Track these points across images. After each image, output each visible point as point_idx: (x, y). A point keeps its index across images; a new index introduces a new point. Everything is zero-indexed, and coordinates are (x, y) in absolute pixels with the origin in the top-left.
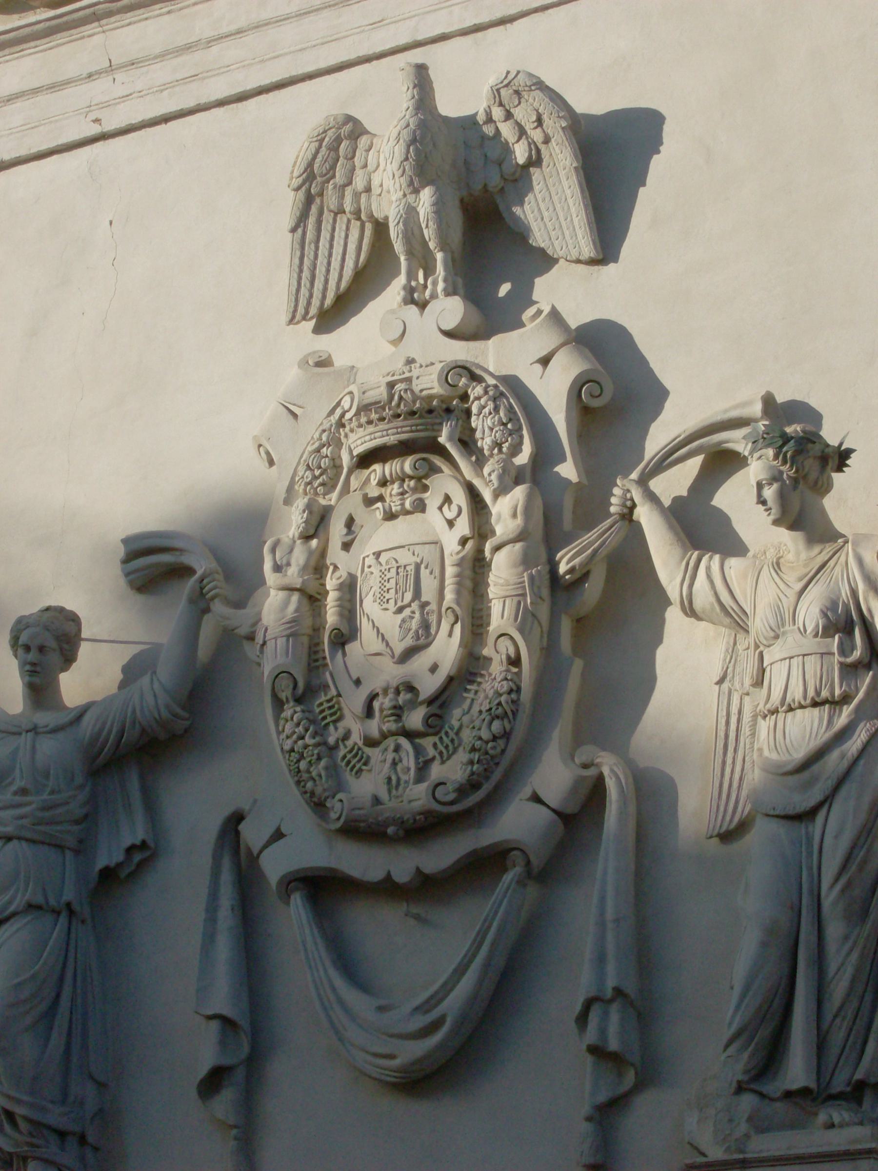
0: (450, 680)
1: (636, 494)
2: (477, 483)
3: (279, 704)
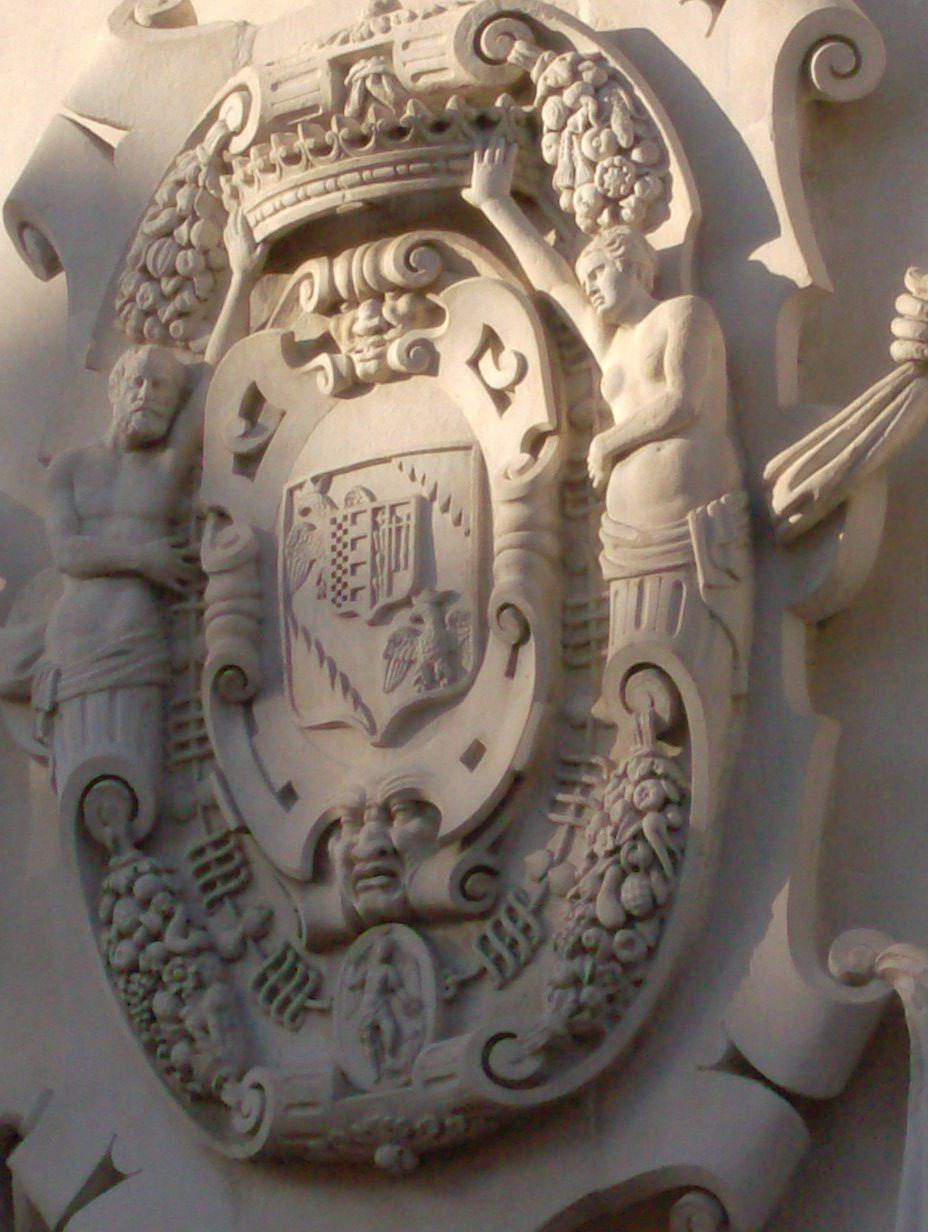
0: (516, 780)
2: (561, 295)
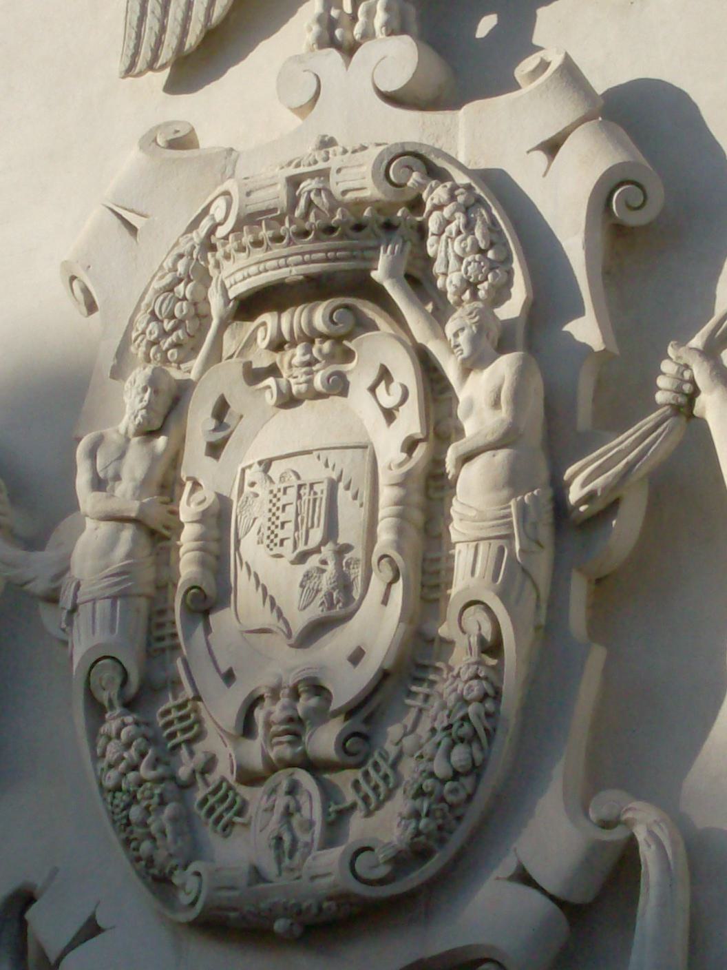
0: (384, 676)
1: (700, 373)
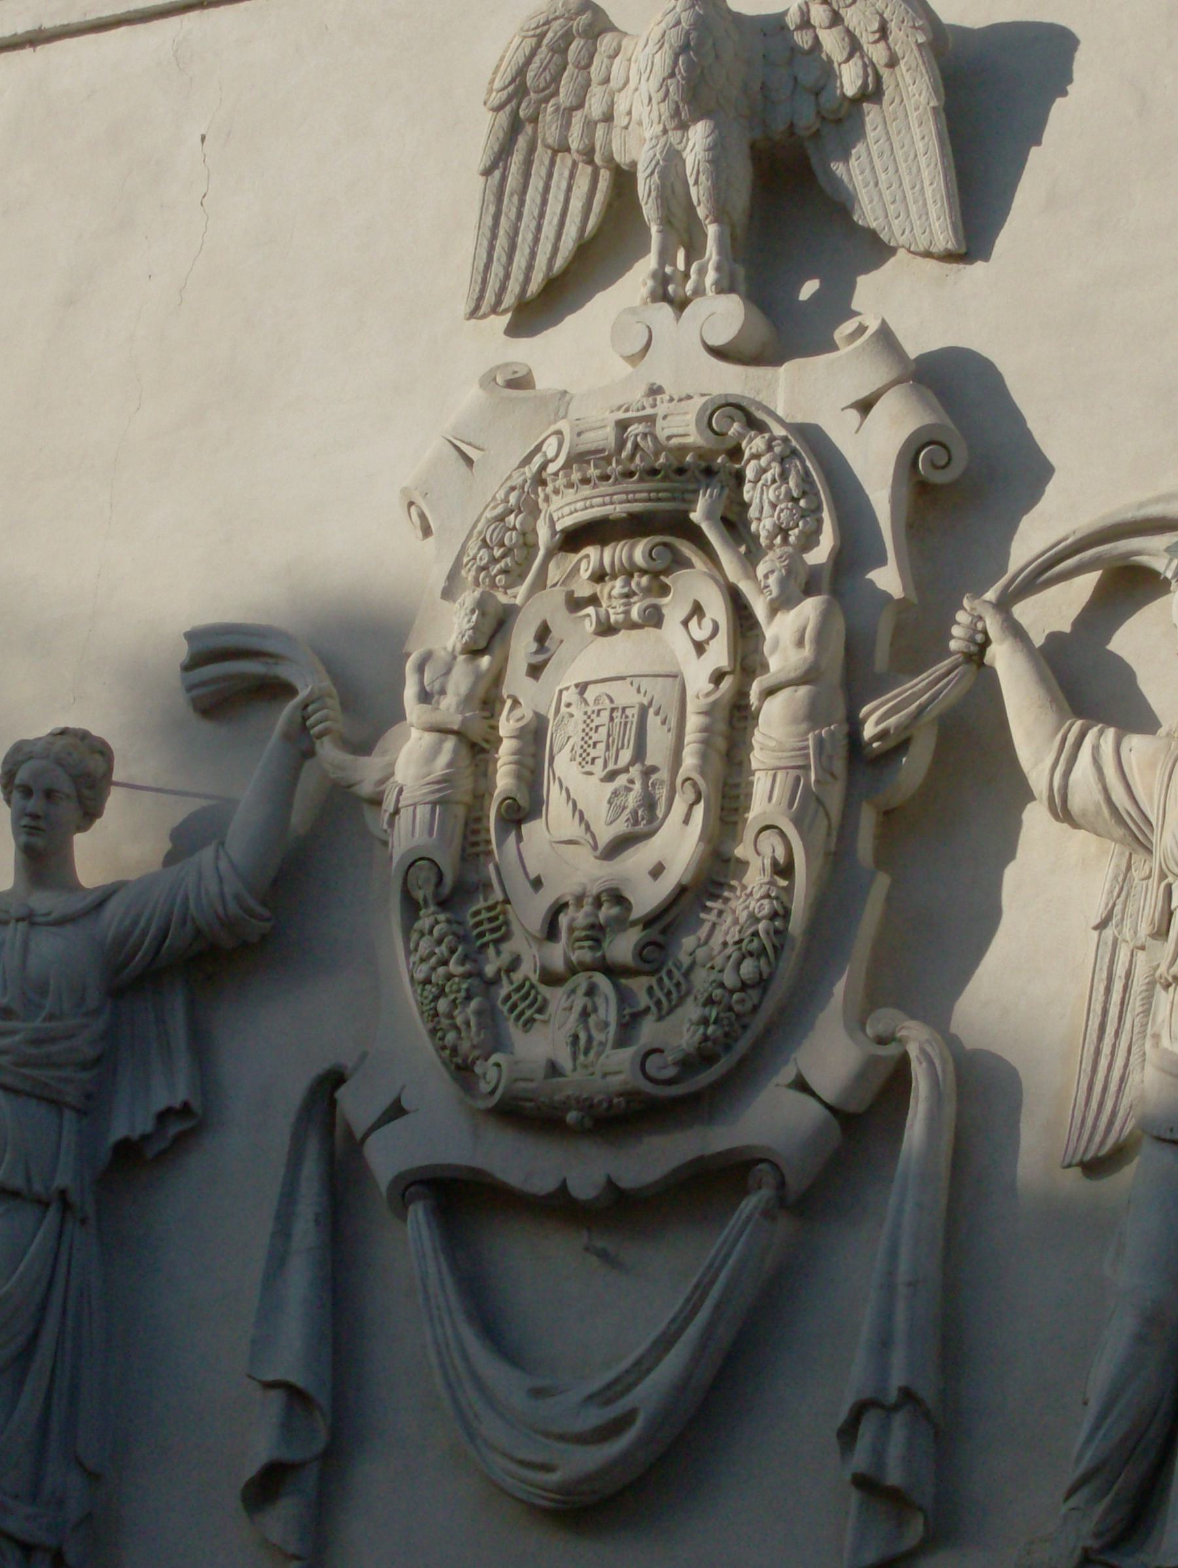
0: (681, 891)
2: (745, 587)
3: (411, 907)
